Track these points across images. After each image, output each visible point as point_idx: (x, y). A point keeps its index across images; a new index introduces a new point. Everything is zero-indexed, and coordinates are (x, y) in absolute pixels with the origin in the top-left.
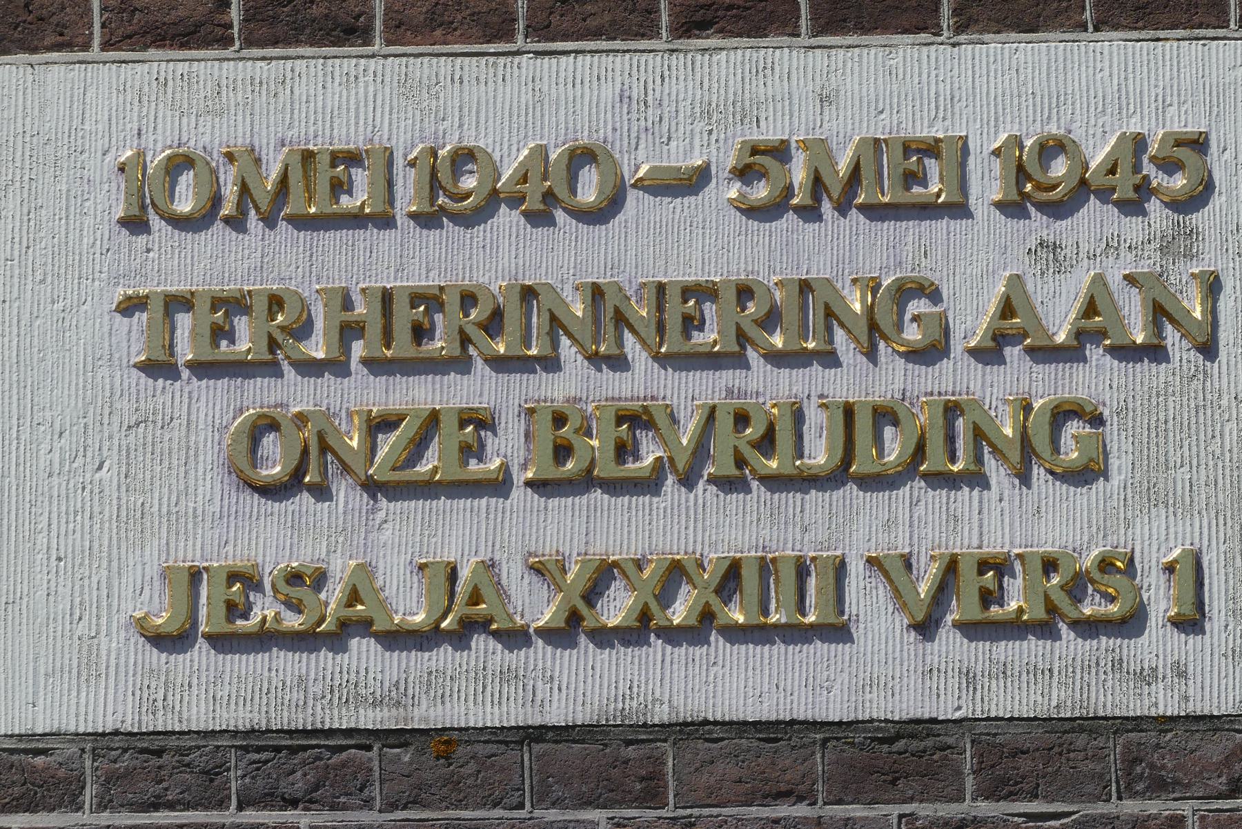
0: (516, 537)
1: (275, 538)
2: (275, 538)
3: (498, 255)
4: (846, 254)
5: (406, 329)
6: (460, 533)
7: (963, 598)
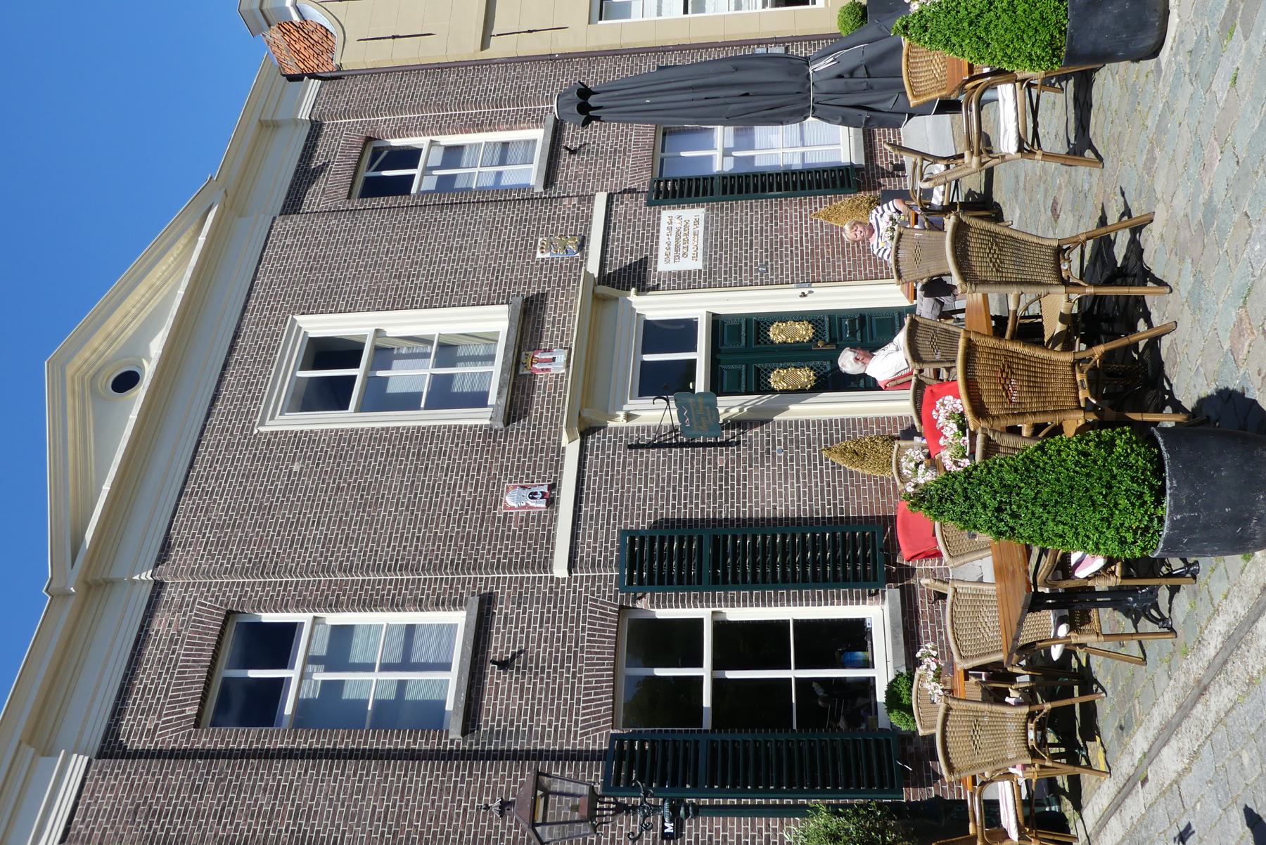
1: (690, 255)
3: (673, 247)
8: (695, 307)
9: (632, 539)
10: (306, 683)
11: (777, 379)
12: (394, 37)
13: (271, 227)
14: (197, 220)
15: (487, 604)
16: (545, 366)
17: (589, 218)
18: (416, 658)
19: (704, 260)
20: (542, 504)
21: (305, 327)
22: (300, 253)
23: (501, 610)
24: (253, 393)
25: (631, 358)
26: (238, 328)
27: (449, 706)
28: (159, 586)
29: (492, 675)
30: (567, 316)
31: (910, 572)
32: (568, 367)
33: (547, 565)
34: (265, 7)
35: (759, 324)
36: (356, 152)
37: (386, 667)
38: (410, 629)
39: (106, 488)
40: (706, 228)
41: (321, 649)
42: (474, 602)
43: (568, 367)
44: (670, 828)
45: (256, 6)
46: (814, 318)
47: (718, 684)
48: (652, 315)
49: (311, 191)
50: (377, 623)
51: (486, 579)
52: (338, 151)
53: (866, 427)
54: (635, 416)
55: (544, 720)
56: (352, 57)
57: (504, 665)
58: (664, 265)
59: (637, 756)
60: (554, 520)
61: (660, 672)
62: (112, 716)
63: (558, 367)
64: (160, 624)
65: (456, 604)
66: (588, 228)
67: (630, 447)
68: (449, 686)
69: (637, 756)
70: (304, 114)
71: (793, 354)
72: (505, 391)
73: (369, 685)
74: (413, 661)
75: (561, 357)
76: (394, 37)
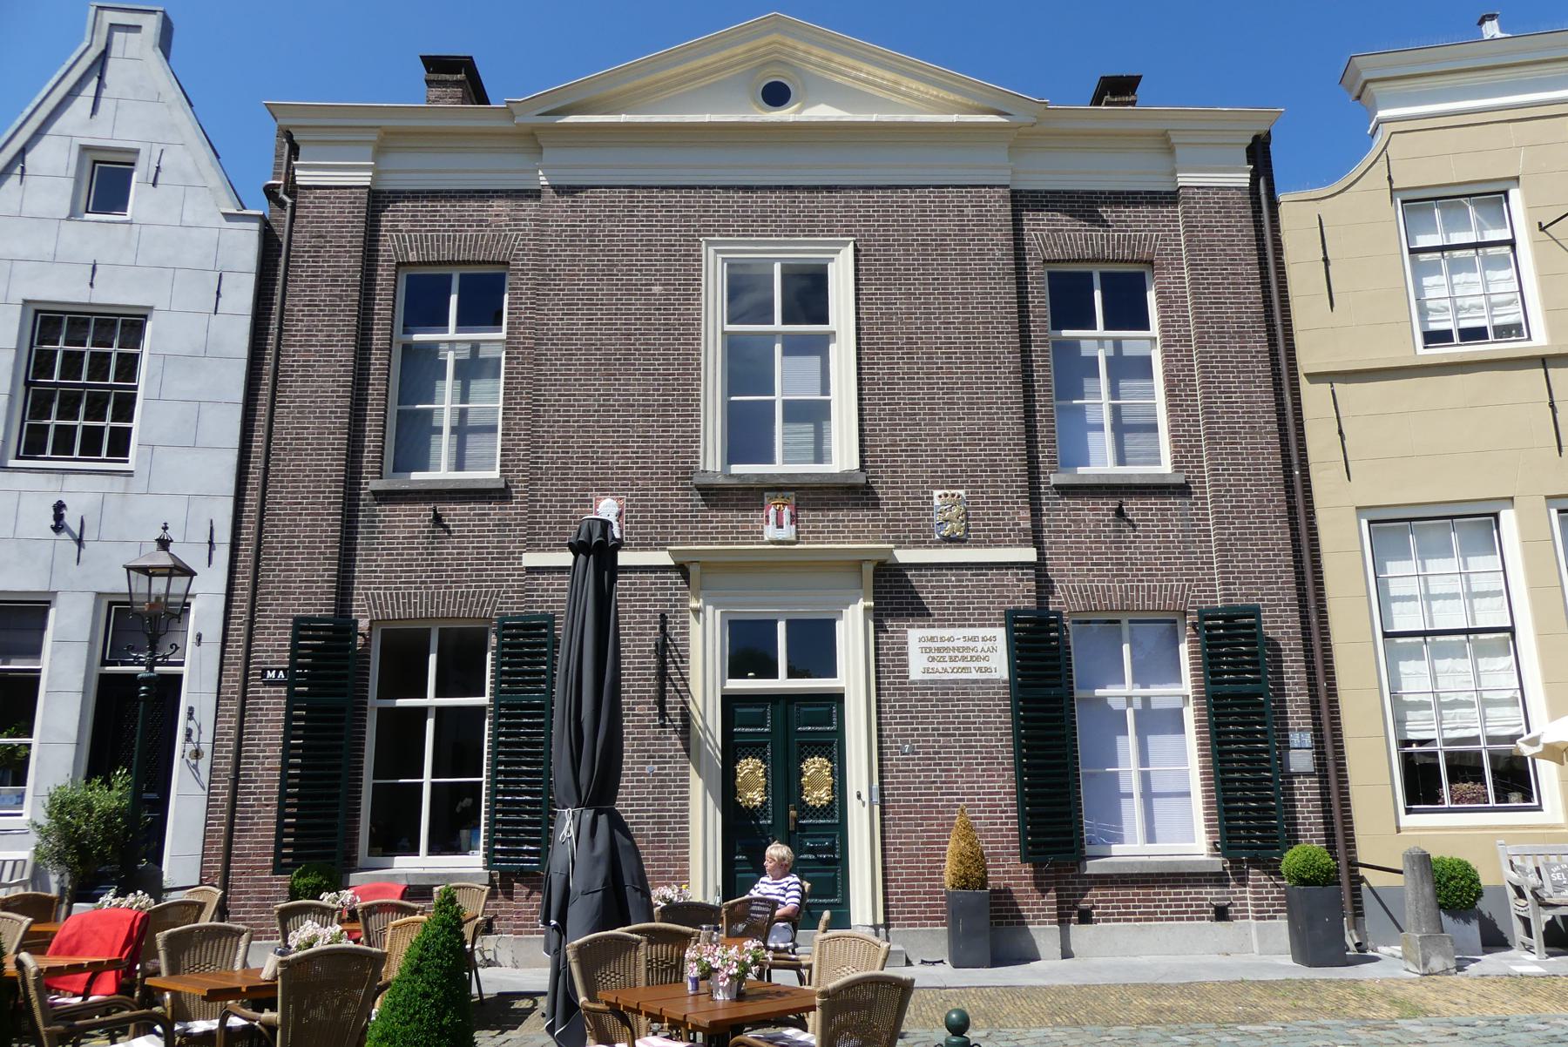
0: (949, 665)
1: (931, 665)
2: (931, 665)
3: (946, 644)
4: (971, 644)
5: (939, 650)
6: (944, 665)
7: (980, 670)
8: (851, 674)
9: (545, 626)
10: (446, 346)
11: (750, 768)
12: (1326, 260)
13: (991, 187)
14: (987, 105)
15: (1183, 490)
16: (772, 519)
17: (997, 544)
19: (922, 682)
21: (839, 258)
22: (951, 226)
23: (494, 510)
24: (748, 226)
25: (780, 609)
26: (844, 188)
27: (1081, 470)
28: (536, 194)
29: (425, 510)
30: (850, 536)
31: (1242, 882)
32: (772, 542)
33: (532, 546)
34: (1370, 86)
35: (832, 747)
36: (1127, 254)
37: (1116, 410)
38: (1153, 428)
39: (623, 118)
40: (975, 681)
41: (1129, 350)
42: (1180, 479)
43: (772, 542)
45: (1365, 76)
46: (837, 806)
47: (422, 712)
48: (840, 627)
49: (1059, 216)
50: (490, 399)
51: (519, 489)
52: (1129, 232)
53: (677, 860)
54: (697, 619)
55: (383, 560)
56: (1297, 216)
57: (438, 519)
58: (916, 637)
59: (1043, 636)
61: (433, 659)
62: (413, 192)
63: (770, 532)
64: (500, 206)
65: (1178, 465)
66: (978, 544)
67: (663, 616)
68: (1102, 463)
69: (1043, 636)
70: (1184, 179)
71: (786, 783)
72: (734, 481)
73: (445, 403)
74: (1126, 436)
75: (788, 532)
76: (1326, 260)
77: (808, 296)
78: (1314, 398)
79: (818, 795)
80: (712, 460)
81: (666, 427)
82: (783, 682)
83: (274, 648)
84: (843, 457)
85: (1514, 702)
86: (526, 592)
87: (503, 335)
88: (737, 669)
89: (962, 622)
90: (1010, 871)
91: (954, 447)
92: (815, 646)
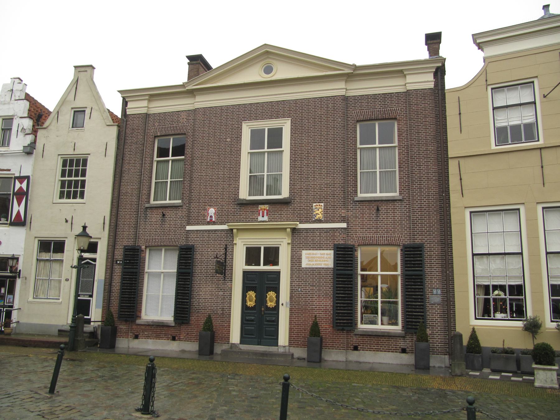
1: (310, 263)
3: (314, 256)
4: (322, 256)
5: (312, 257)
8: (284, 266)
17: (333, 222)
18: (374, 207)
20: (208, 220)
33: (189, 224)
35: (277, 290)
42: (401, 198)
44: (118, 262)
46: (276, 308)
47: (377, 275)
60: (203, 224)
63: (260, 218)
67: (226, 245)
77: (275, 137)
78: (453, 166)
79: (271, 304)
80: (244, 194)
81: (230, 185)
82: (262, 267)
83: (119, 255)
84: (285, 193)
85: (552, 277)
86: (187, 238)
87: (396, 144)
88: (248, 263)
89: (320, 248)
90: (326, 327)
91: (321, 189)
92: (272, 255)
